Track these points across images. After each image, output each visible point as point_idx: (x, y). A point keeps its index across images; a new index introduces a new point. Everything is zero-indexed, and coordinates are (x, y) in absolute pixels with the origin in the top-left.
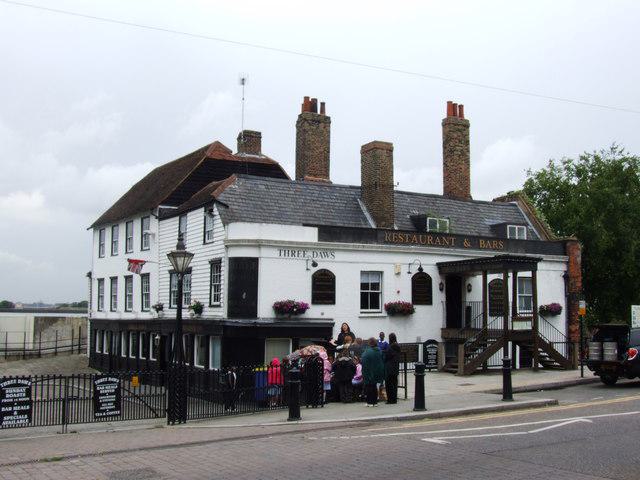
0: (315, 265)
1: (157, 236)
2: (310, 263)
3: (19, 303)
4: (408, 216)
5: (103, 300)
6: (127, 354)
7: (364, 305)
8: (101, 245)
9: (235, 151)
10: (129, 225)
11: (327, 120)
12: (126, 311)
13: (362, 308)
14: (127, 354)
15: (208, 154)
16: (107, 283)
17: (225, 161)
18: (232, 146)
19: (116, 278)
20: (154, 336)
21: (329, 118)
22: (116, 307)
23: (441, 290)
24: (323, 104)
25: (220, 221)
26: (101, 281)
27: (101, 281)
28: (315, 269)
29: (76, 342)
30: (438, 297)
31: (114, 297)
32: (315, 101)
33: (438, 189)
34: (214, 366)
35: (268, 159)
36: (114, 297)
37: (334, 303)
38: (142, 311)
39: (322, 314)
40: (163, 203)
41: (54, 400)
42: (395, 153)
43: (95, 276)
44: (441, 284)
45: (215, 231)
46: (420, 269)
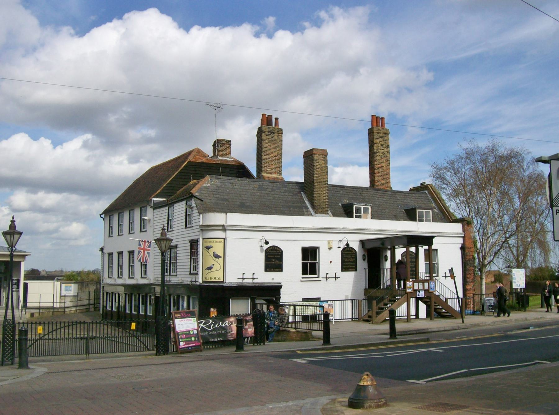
0: (267, 243)
1: (152, 221)
2: (263, 241)
3: (43, 270)
4: (340, 204)
5: (112, 269)
6: (131, 310)
7: (305, 272)
8: (111, 227)
9: (211, 154)
10: (131, 212)
11: (280, 131)
12: (129, 278)
13: (303, 274)
14: (131, 310)
15: (191, 158)
16: (115, 256)
17: (203, 163)
18: (208, 150)
19: (122, 252)
20: (150, 297)
21: (281, 130)
22: (122, 275)
23: (364, 260)
24: (277, 119)
25: (197, 211)
26: (110, 254)
27: (110, 254)
28: (266, 247)
29: (92, 302)
30: (362, 265)
31: (120, 266)
32: (270, 117)
33: (367, 184)
34: (150, 313)
35: (236, 161)
36: (120, 266)
37: (281, 271)
38: (142, 277)
39: (273, 279)
40: (157, 196)
41: (81, 339)
42: (329, 158)
43: (105, 251)
44: (364, 255)
45: (193, 215)
46: (347, 245)
